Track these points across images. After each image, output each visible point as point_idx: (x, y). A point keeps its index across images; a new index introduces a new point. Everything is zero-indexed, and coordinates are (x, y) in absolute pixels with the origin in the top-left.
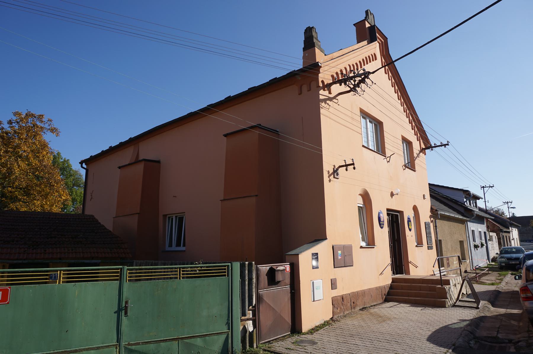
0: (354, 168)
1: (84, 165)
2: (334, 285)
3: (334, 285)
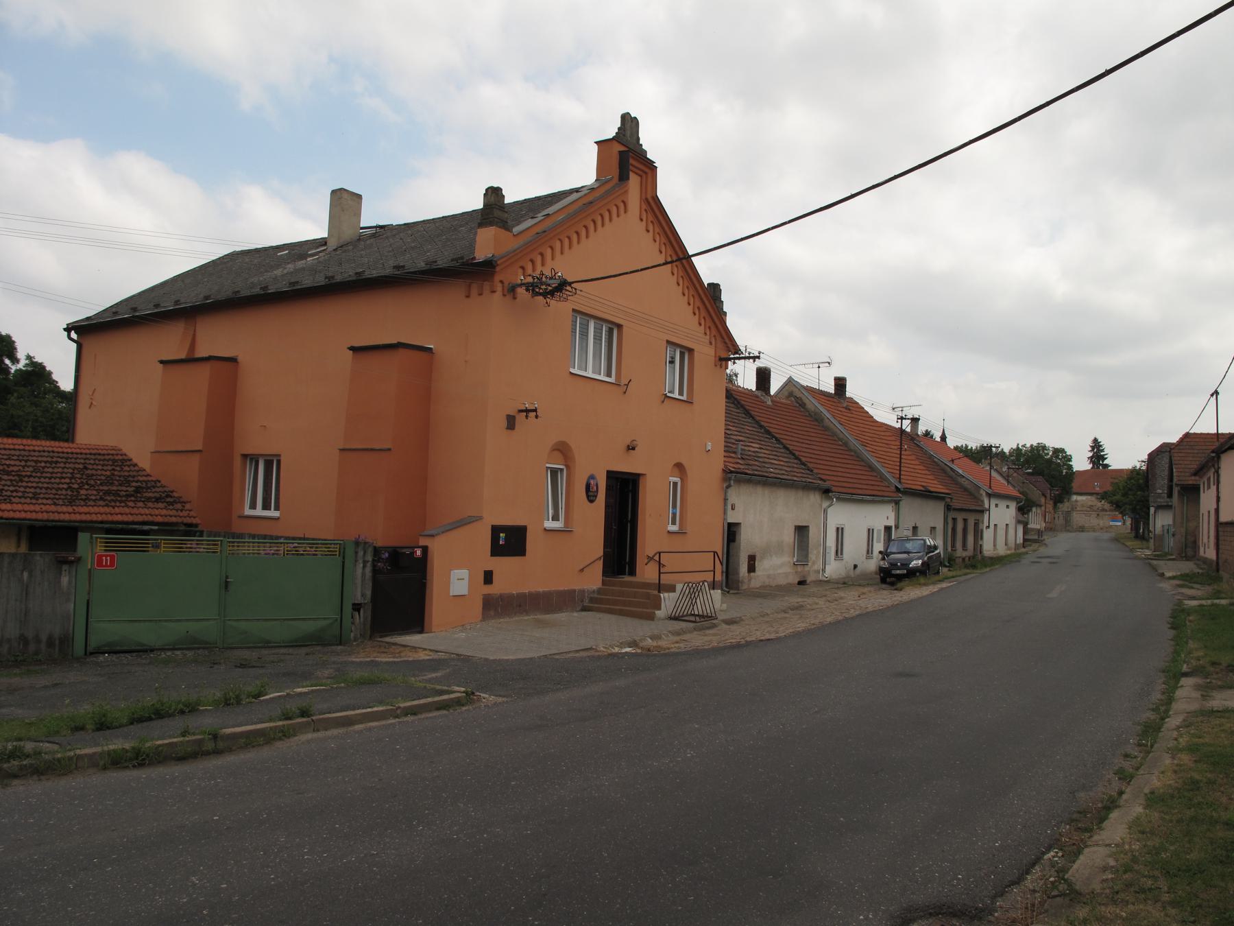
0: (537, 417)
1: (74, 335)
2: (488, 577)
3: (488, 577)
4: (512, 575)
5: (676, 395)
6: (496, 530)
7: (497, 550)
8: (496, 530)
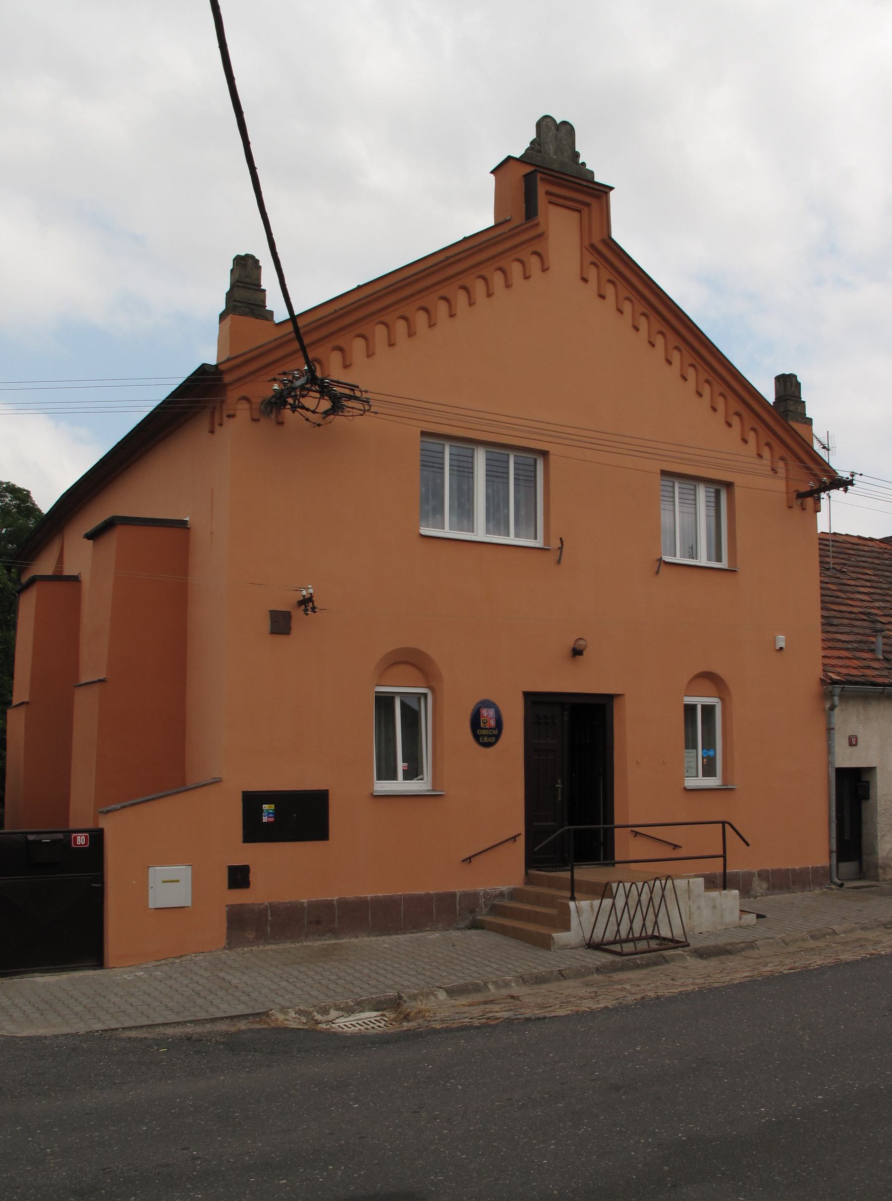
2: (239, 877)
3: (239, 877)
4: (286, 872)
5: (703, 560)
6: (252, 802)
7: (254, 831)
8: (252, 802)
